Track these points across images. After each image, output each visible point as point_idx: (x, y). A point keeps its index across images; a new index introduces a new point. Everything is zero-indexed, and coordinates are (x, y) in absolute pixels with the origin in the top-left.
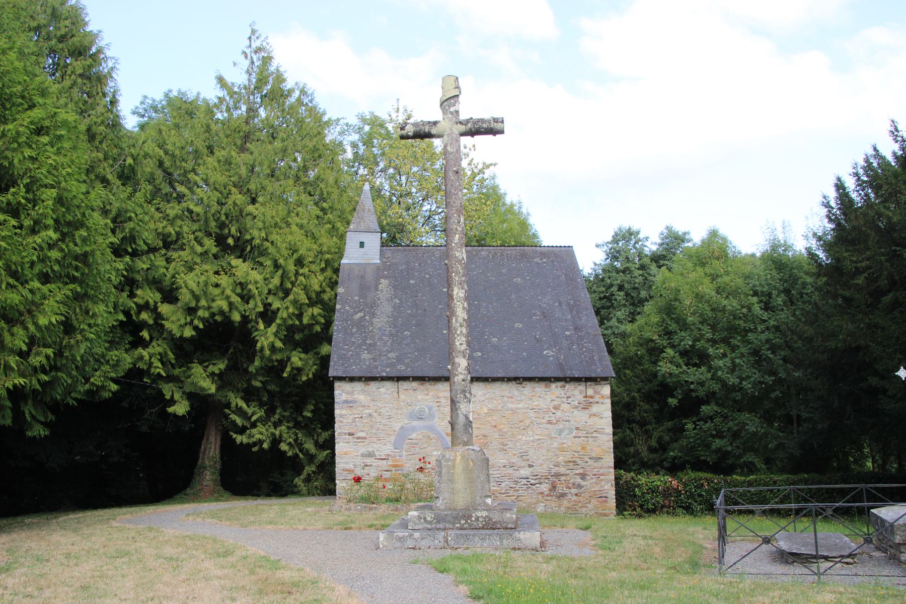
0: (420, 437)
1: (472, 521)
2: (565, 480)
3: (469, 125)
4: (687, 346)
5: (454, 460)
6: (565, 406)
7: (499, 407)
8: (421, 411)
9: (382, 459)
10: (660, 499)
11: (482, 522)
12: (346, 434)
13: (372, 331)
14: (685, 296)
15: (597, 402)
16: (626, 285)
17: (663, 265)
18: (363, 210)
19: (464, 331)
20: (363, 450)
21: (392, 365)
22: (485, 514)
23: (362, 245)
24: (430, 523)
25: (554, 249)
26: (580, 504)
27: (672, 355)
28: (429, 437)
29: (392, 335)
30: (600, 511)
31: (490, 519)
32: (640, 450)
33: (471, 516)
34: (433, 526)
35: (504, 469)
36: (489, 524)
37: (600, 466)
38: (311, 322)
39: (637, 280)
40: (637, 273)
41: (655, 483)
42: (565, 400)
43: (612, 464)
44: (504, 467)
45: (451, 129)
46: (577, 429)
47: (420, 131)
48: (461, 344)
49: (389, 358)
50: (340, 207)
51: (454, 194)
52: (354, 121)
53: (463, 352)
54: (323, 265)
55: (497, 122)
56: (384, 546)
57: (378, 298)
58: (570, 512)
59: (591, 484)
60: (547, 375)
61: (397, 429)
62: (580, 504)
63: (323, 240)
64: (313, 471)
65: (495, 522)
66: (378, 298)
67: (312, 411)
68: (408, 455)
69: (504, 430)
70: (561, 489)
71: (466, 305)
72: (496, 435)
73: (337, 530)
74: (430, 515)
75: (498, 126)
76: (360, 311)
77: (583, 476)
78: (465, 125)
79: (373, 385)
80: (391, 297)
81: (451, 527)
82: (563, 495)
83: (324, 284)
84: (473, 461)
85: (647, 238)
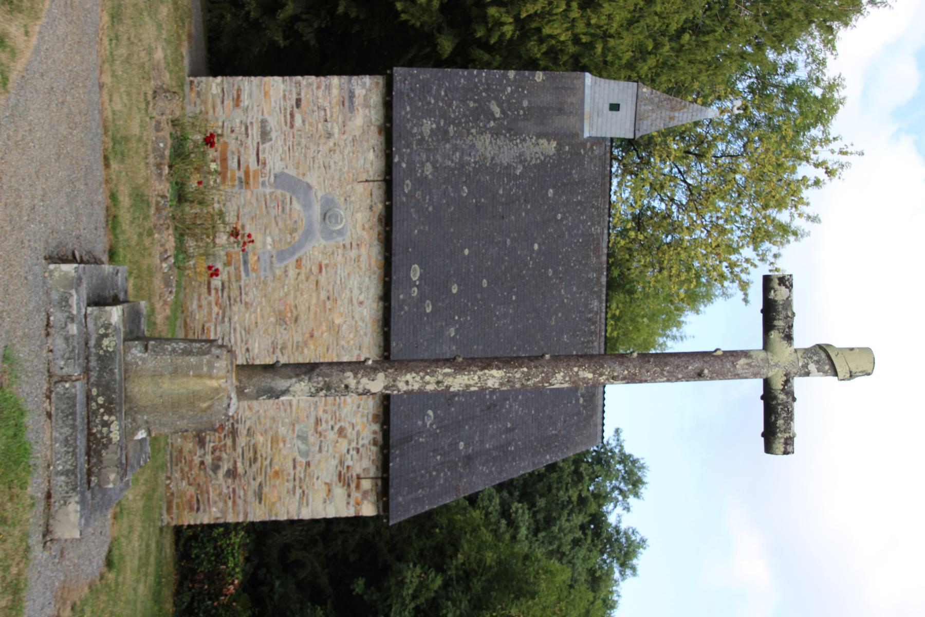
0: (295, 216)
1: (103, 415)
2: (225, 445)
3: (782, 396)
4: (445, 611)
5: (211, 377)
6: (343, 445)
7: (342, 343)
8: (337, 218)
9: (258, 154)
10: (205, 567)
11: (101, 432)
12: (299, 94)
13: (469, 133)
14: (524, 608)
15: (349, 496)
16: (554, 475)
17: (585, 534)
18: (673, 109)
19: (430, 388)
20: (272, 123)
21: (411, 169)
22: (115, 436)
23: (615, 107)
24: (99, 345)
25: (599, 414)
26: (187, 469)
27: (431, 586)
28: (293, 230)
29: (463, 166)
30: (175, 501)
31: (106, 446)
32: (284, 533)
33: (110, 413)
34: (93, 350)
35: (244, 350)
36: (98, 444)
37: (248, 500)
38: (490, 20)
39: (561, 493)
40: (574, 494)
41: (231, 559)
42: (354, 445)
43: (251, 518)
44: (248, 350)
45: (776, 365)
46: (308, 464)
47: (775, 311)
48: (407, 382)
49: (423, 165)
50: (682, 64)
51: (663, 370)
52: (830, 72)
53: (393, 386)
54: (584, 39)
55: (786, 444)
56: (51, 272)
57: (524, 140)
58: (175, 454)
59: (220, 485)
60: (394, 419)
61: (307, 179)
62: (187, 469)
63: (627, 39)
64: (248, 13)
65: (101, 455)
66: (524, 140)
67: (346, 14)
68: (265, 196)
69: (306, 351)
70: (212, 440)
71: (473, 389)
72: (298, 337)
73: (103, 142)
74: (113, 344)
75: (779, 445)
76: (503, 112)
77: (232, 474)
78: (783, 390)
79: (375, 139)
80: (526, 160)
81: (92, 380)
82: (202, 443)
83: (553, 42)
84: (209, 407)
85: (627, 509)
